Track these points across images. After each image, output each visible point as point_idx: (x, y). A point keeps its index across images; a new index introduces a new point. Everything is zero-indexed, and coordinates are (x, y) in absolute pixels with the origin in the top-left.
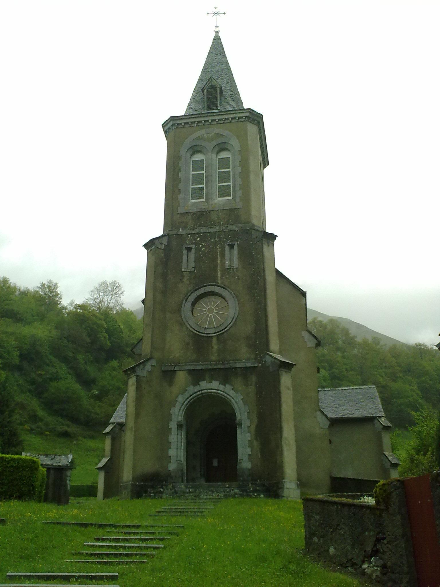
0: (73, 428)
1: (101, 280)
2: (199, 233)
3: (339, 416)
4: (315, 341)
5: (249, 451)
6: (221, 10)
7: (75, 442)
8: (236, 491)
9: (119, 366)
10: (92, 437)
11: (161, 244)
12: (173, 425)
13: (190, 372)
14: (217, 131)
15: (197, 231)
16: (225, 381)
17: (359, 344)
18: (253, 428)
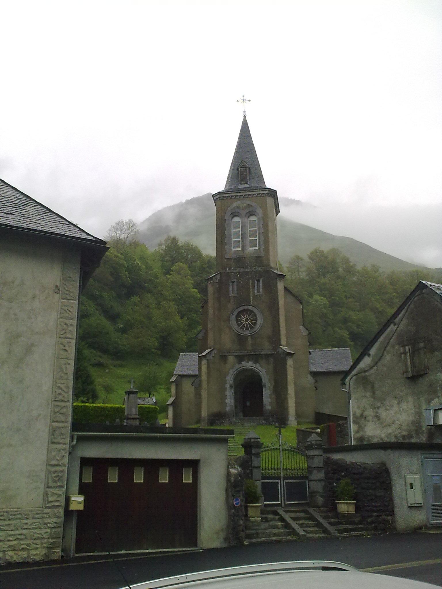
0: (105, 359)
1: (117, 220)
2: (239, 272)
3: (324, 370)
4: (307, 332)
5: (270, 400)
6: (247, 98)
7: (107, 371)
8: (264, 421)
9: (139, 301)
10: (121, 366)
11: (217, 279)
12: (228, 386)
13: (236, 356)
14: (248, 202)
15: (237, 271)
16: (256, 362)
17: (358, 272)
18: (272, 387)
